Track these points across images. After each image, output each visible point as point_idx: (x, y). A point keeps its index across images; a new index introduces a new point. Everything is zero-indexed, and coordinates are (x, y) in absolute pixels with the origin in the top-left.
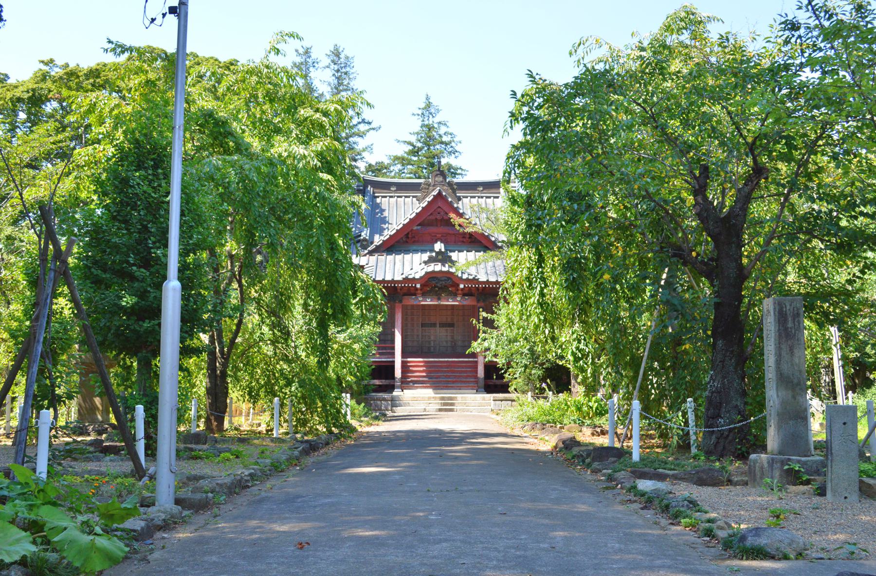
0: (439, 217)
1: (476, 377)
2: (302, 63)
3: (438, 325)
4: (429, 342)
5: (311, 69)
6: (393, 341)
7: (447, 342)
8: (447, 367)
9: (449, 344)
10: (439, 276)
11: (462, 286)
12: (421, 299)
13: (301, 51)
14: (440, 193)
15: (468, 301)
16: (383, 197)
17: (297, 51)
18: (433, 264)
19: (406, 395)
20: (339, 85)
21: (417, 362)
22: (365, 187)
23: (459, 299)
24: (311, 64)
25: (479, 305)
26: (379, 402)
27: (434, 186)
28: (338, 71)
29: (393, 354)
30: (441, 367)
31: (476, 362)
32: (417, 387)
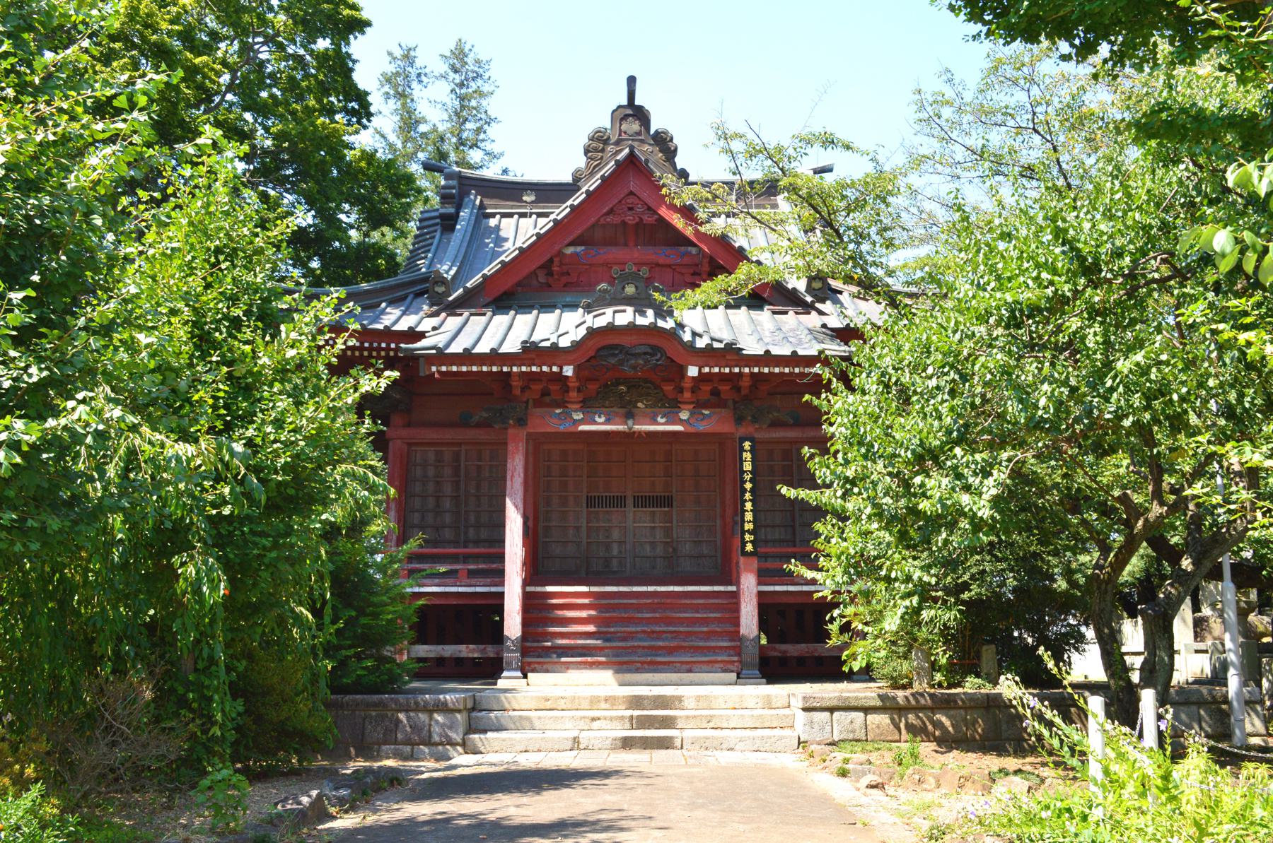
0: (630, 219)
1: (735, 635)
2: (398, 74)
3: (630, 501)
4: (608, 546)
5: (414, 85)
6: (499, 541)
7: (653, 544)
8: (652, 608)
9: (659, 550)
10: (626, 341)
11: (693, 371)
12: (578, 416)
13: (398, 53)
14: (632, 156)
15: (711, 422)
16: (504, 215)
17: (390, 54)
18: (609, 311)
19: (522, 691)
20: (461, 114)
21: (568, 594)
22: (463, 194)
23: (684, 415)
24: (413, 76)
25: (742, 431)
26: (423, 717)
27: (618, 143)
28: (461, 85)
29: (499, 575)
30: (638, 608)
31: (735, 596)
32: (568, 666)
